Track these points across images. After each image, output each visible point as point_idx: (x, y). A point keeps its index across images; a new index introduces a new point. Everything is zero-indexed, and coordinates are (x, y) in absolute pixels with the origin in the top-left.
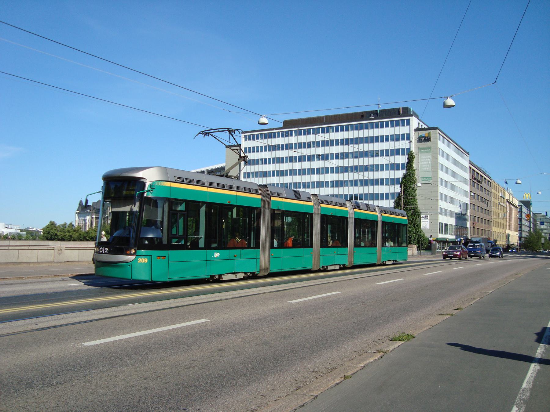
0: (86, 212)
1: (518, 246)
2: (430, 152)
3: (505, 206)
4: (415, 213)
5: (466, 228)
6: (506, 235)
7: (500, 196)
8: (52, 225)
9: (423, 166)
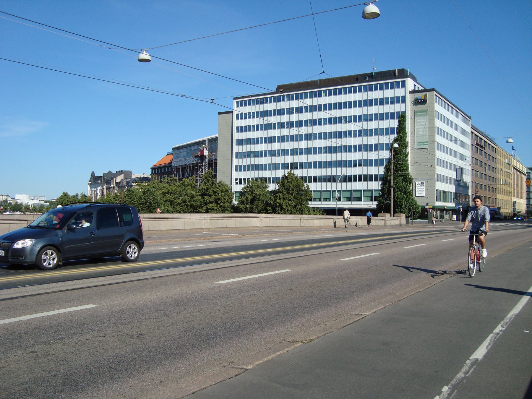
0: (97, 183)
1: (525, 213)
3: (512, 173)
4: (406, 180)
5: (468, 195)
6: (512, 202)
7: (506, 163)
8: (65, 196)
9: (419, 130)
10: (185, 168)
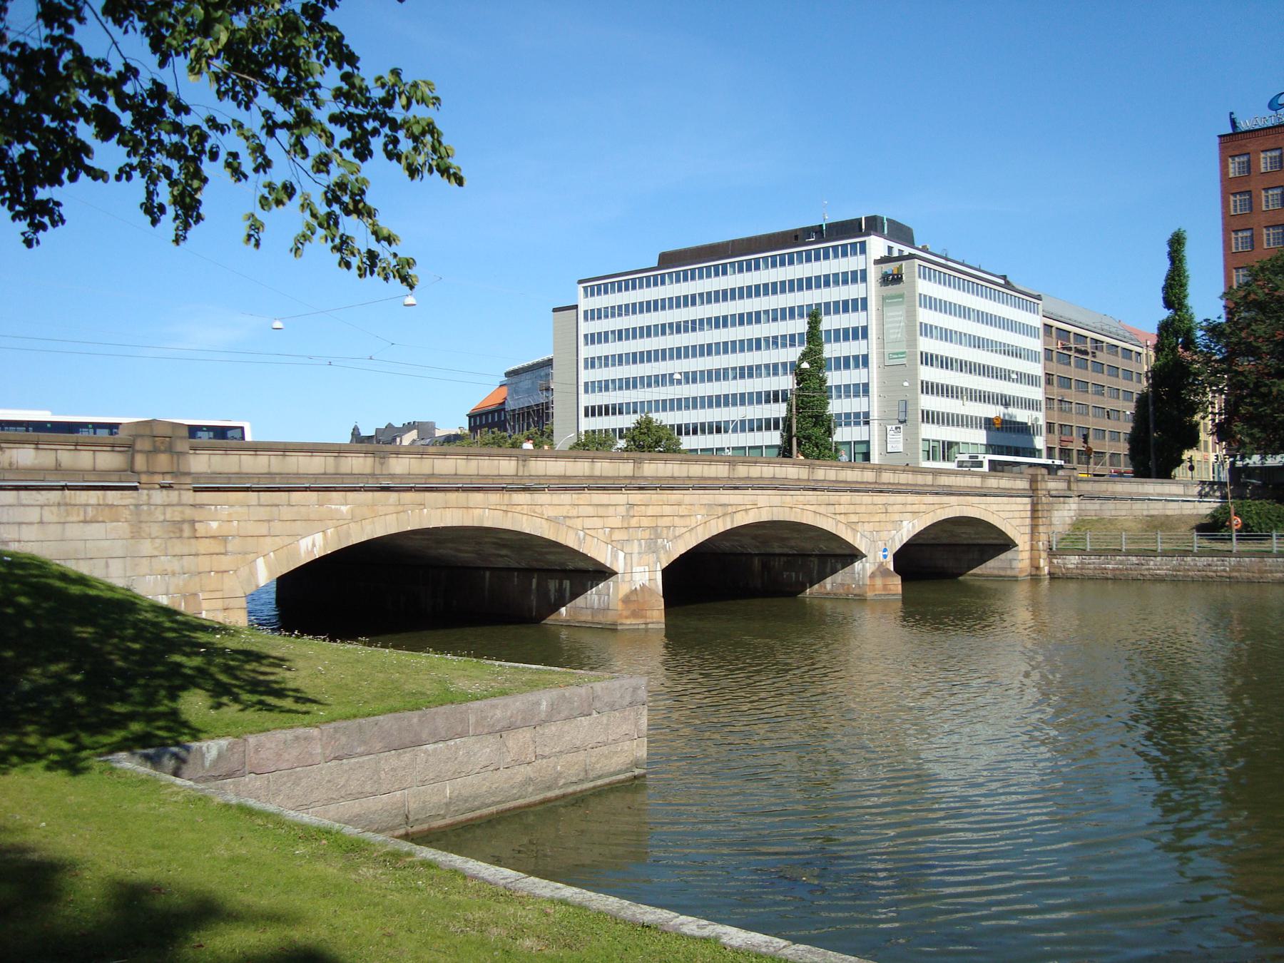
2: (901, 303)
10: (528, 413)
